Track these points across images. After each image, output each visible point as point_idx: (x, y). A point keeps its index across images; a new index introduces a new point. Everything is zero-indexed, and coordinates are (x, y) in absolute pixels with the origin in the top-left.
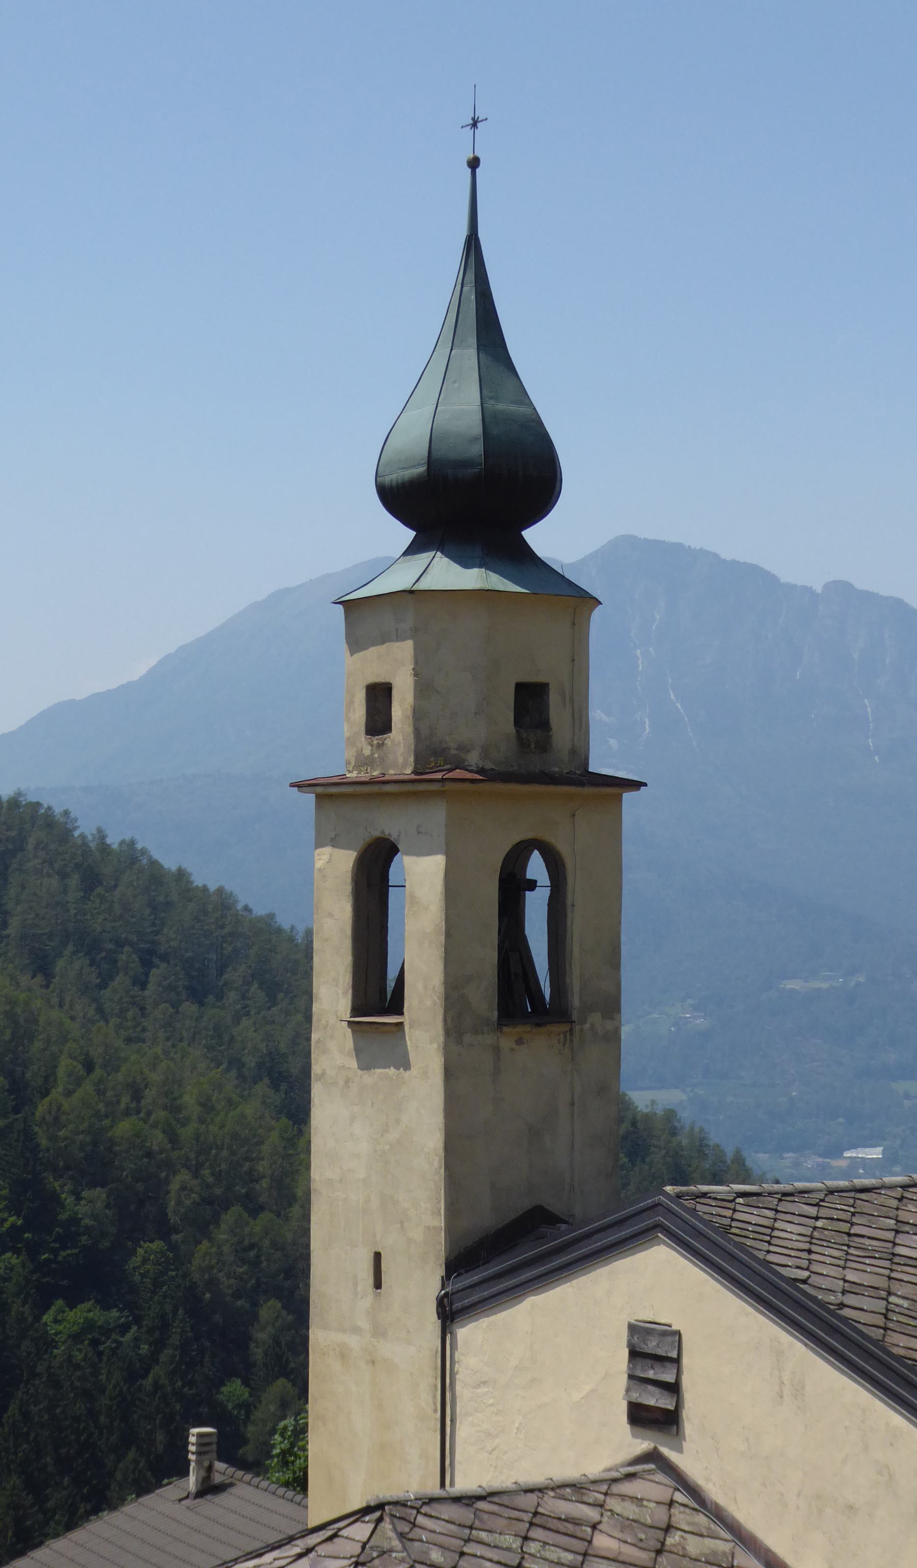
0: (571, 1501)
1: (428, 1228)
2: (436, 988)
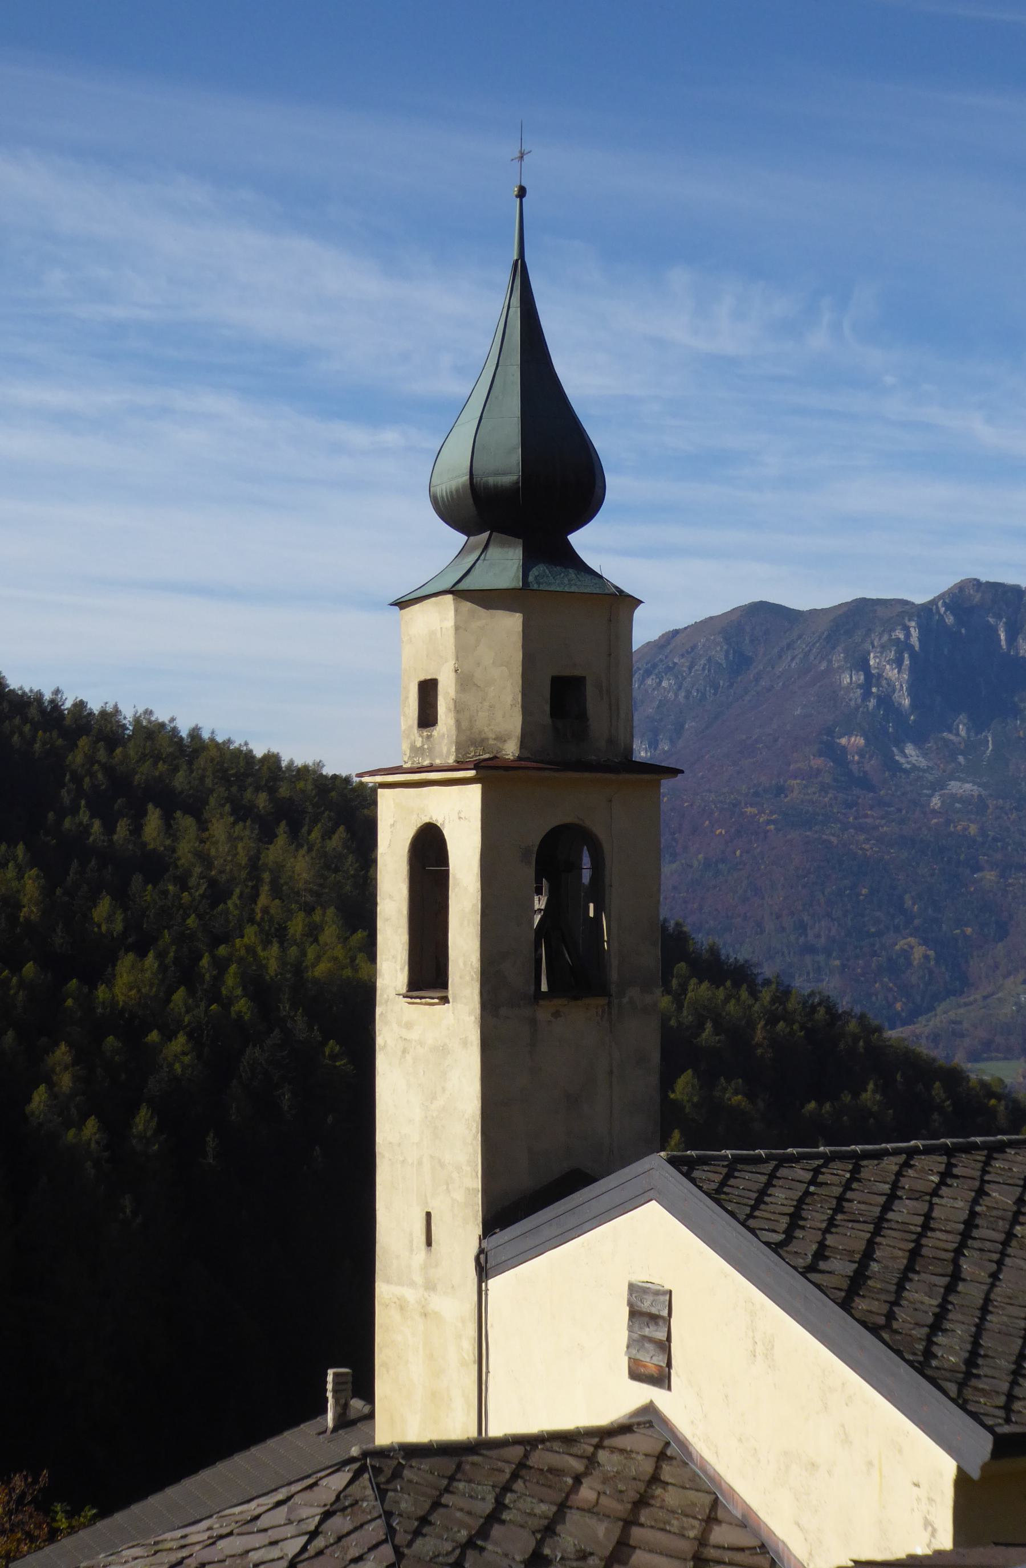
0: (558, 1452)
1: (468, 1189)
2: (473, 964)
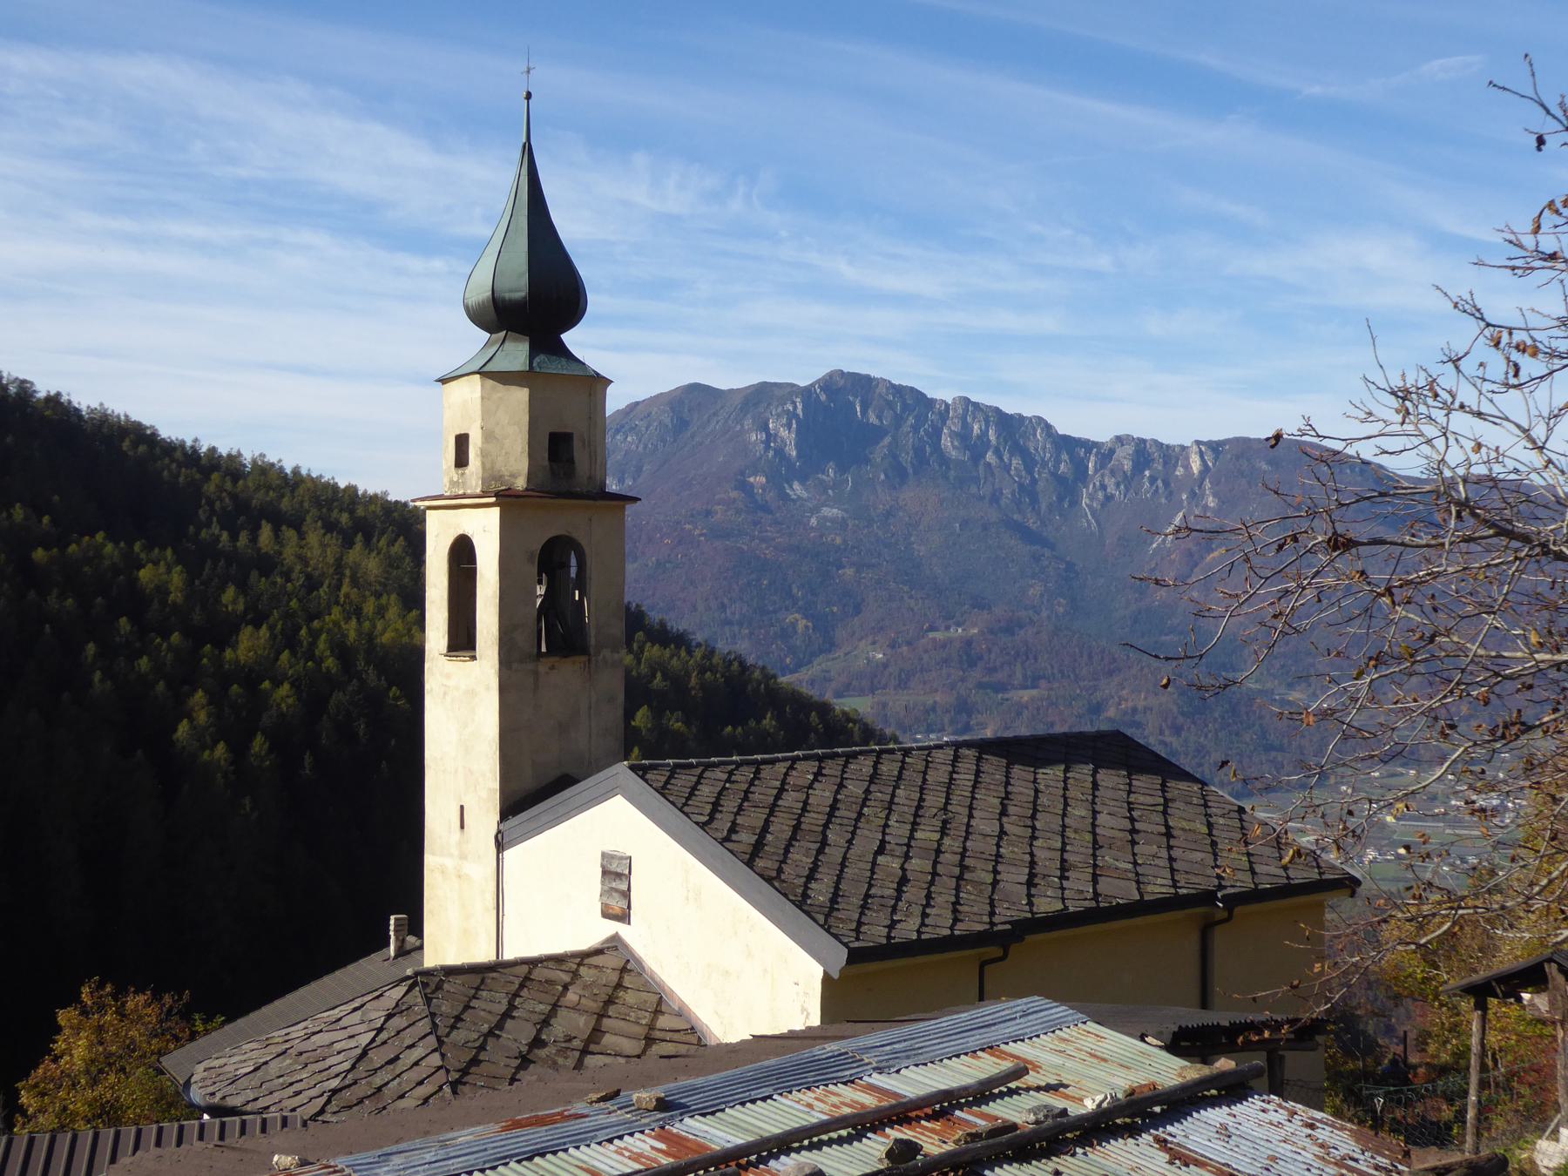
1: (490, 789)
